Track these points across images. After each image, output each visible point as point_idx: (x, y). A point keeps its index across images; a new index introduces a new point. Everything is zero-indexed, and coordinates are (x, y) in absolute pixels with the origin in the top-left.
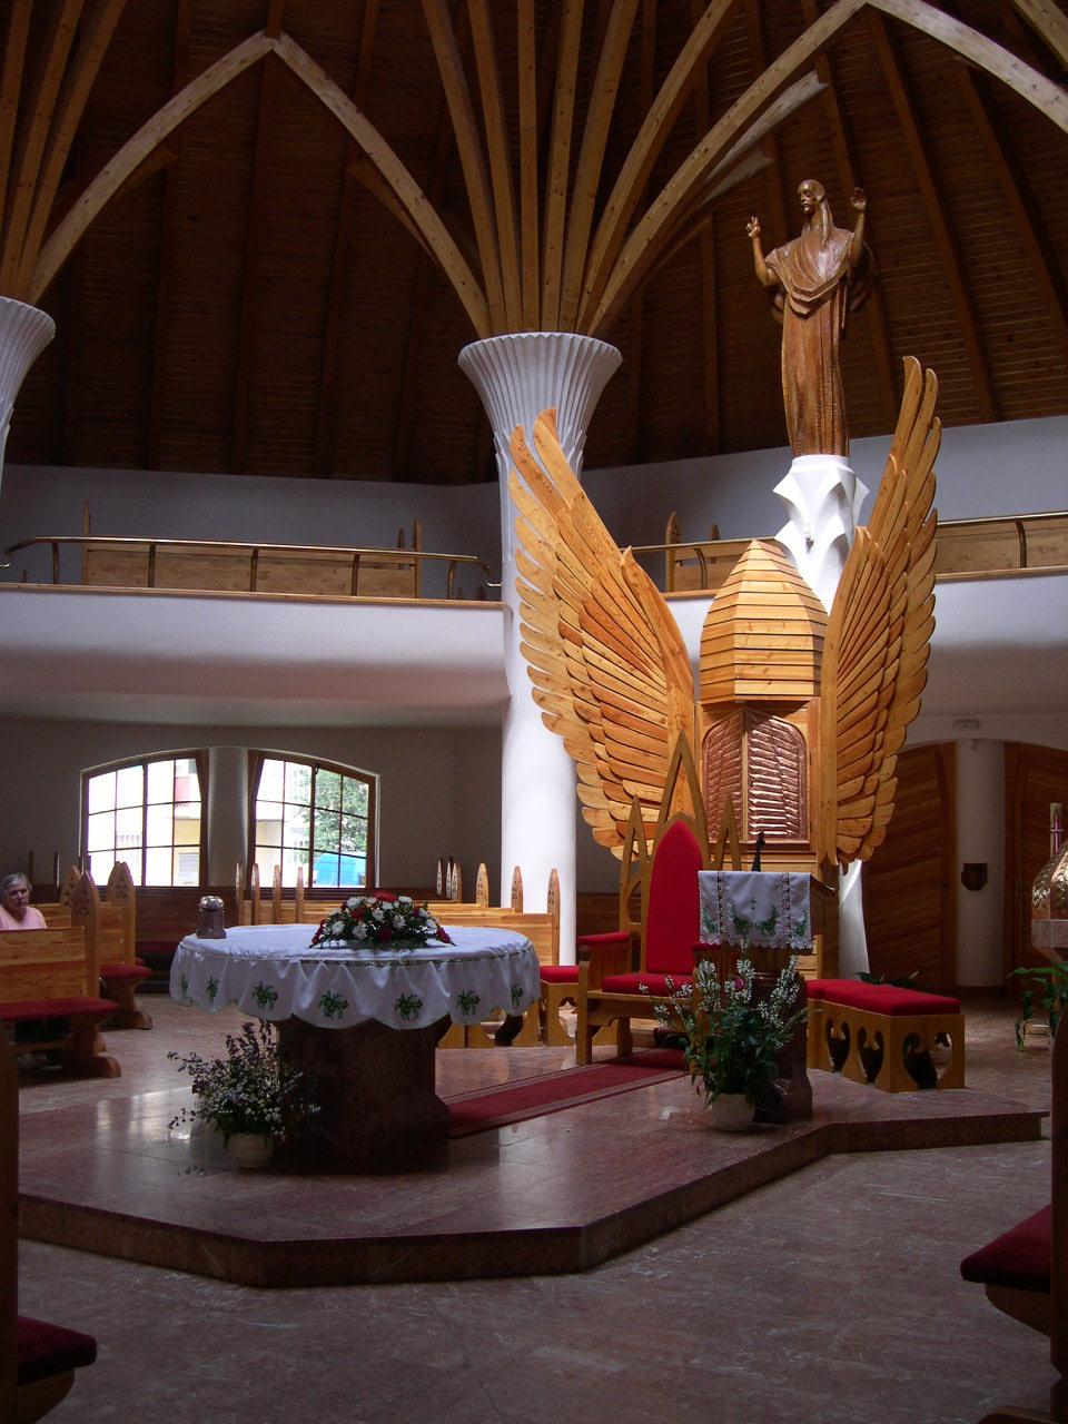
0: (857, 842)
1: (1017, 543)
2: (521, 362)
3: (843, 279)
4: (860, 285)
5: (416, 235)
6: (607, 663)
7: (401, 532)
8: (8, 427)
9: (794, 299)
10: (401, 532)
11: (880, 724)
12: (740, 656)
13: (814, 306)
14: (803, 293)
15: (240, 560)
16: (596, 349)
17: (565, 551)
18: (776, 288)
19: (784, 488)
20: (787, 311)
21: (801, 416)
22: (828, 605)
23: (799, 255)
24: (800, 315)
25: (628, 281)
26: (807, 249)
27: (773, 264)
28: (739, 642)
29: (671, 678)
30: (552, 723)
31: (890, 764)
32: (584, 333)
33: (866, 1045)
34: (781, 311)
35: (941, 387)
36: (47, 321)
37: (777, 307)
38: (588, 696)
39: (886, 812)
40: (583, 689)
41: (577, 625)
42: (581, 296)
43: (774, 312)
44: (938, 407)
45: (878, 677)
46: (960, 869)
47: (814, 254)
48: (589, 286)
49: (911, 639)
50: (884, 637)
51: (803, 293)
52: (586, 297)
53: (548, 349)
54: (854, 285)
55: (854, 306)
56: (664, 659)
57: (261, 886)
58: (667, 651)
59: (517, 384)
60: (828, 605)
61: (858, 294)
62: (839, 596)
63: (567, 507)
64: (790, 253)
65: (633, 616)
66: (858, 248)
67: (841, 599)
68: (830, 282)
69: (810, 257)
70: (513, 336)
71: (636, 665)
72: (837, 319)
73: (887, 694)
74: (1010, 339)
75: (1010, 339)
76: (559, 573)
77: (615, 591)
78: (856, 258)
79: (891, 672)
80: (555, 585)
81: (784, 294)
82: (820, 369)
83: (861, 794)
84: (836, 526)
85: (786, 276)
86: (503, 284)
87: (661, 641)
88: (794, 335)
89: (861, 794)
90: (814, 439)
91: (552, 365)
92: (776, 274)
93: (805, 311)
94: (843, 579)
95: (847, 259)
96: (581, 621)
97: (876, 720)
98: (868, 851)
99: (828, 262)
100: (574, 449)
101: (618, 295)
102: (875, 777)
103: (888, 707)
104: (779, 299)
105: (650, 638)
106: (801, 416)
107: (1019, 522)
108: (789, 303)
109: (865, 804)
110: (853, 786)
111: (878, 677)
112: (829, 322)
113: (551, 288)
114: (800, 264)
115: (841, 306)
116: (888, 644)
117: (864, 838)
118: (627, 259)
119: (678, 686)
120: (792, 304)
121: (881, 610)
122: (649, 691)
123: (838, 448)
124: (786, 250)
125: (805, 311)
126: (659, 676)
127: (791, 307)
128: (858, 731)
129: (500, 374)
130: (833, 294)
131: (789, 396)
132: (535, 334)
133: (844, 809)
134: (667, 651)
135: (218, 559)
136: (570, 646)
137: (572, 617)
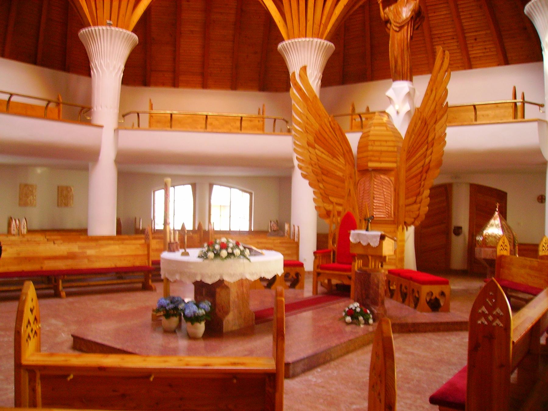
0: (413, 220)
1: (474, 113)
2: (299, 49)
3: (412, 18)
4: (418, 20)
5: (264, 6)
6: (325, 156)
7: (259, 109)
8: (122, 74)
9: (394, 26)
10: (259, 109)
11: (423, 178)
12: (370, 153)
13: (401, 28)
14: (397, 23)
15: (237, 120)
16: (325, 44)
17: (310, 116)
18: (388, 21)
19: (390, 93)
20: (391, 30)
21: (396, 67)
22: (403, 136)
23: (396, 9)
24: (396, 31)
25: (337, 20)
26: (399, 6)
27: (388, 13)
28: (370, 148)
29: (346, 161)
30: (305, 176)
31: (427, 192)
32: (321, 38)
33: (414, 295)
34: (389, 29)
35: (450, 57)
36: (135, 37)
37: (388, 28)
38: (317, 167)
39: (425, 209)
40: (315, 164)
41: (313, 141)
42: (320, 26)
43: (387, 30)
44: (450, 64)
45: (423, 162)
46: (453, 228)
47: (401, 9)
48: (323, 21)
49: (436, 148)
50: (426, 147)
51: (397, 23)
52: (322, 26)
53: (308, 45)
54: (416, 19)
55: (416, 27)
56: (344, 154)
57: (215, 230)
58: (345, 152)
59: (297, 56)
60: (403, 136)
61: (417, 23)
62: (408, 132)
63: (310, 100)
64: (393, 9)
65: (333, 139)
66: (417, 6)
67: (408, 133)
68: (407, 19)
69: (400, 9)
70: (296, 40)
71: (334, 156)
72: (409, 32)
73: (425, 169)
74: (476, 39)
75: (476, 39)
76: (307, 123)
77: (327, 130)
78: (416, 10)
79: (427, 160)
80: (306, 128)
81: (391, 24)
82: (403, 51)
83: (415, 202)
84: (407, 107)
85: (391, 17)
86: (293, 22)
87: (343, 147)
88: (393, 38)
89: (415, 202)
90: (400, 75)
91: (310, 49)
92: (387, 16)
93: (397, 29)
94: (409, 126)
95: (413, 11)
96: (315, 141)
97: (421, 177)
98: (418, 223)
99: (407, 12)
100: (317, 80)
101: (333, 25)
102: (420, 197)
103: (426, 172)
104: (389, 25)
105: (340, 147)
106: (396, 67)
107: (474, 106)
108: (392, 27)
109: (416, 207)
110: (412, 200)
111: (423, 162)
112: (405, 34)
113: (310, 23)
114: (397, 13)
115: (411, 28)
116: (427, 150)
117: (415, 219)
118: (336, 12)
119: (349, 164)
120: (393, 27)
121: (424, 138)
122: (339, 165)
123: (408, 78)
124: (392, 8)
125: (397, 29)
126: (342, 160)
127: (393, 29)
128: (414, 181)
129: (292, 54)
130: (408, 23)
131: (392, 61)
132: (304, 39)
133: (408, 208)
134: (345, 152)
135: (423, 121)
136: (311, 149)
137: (311, 139)
